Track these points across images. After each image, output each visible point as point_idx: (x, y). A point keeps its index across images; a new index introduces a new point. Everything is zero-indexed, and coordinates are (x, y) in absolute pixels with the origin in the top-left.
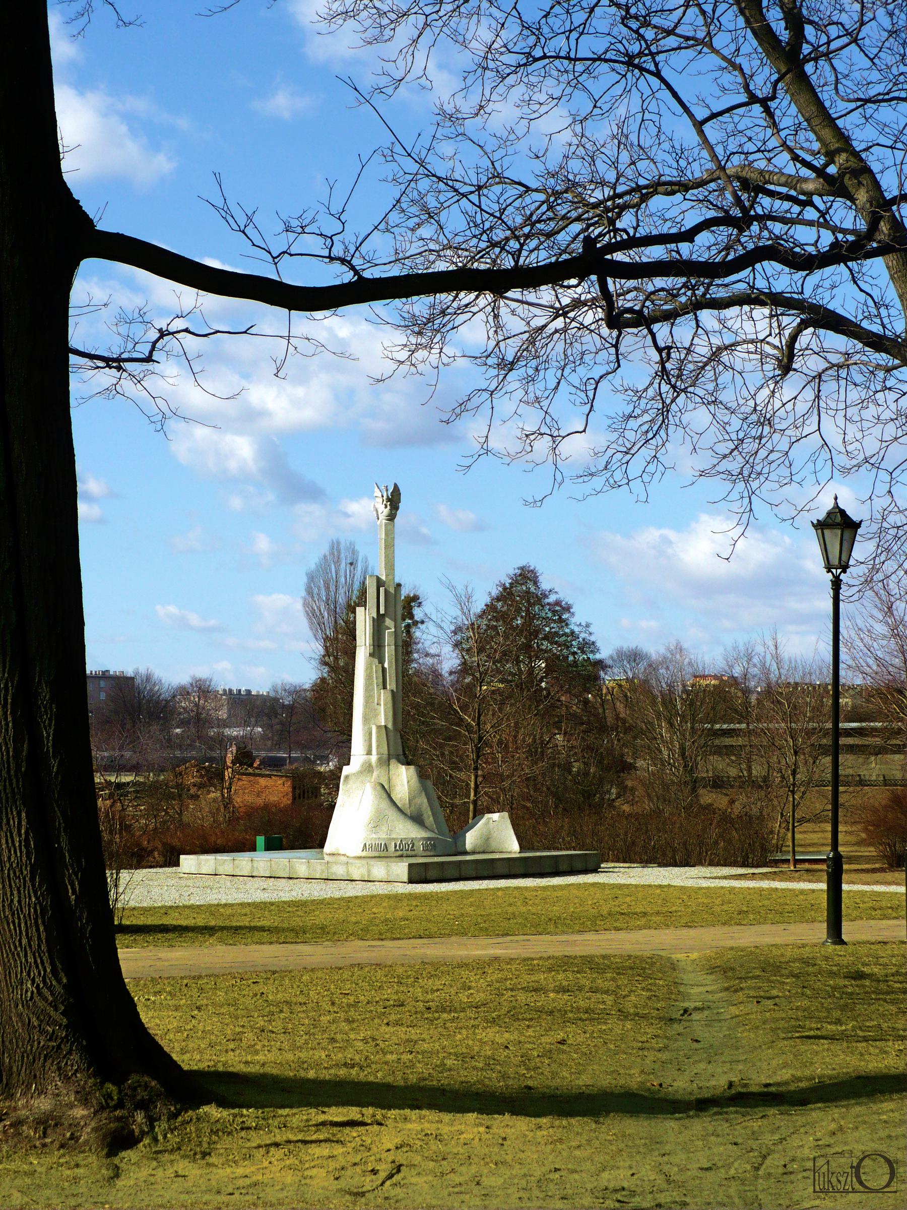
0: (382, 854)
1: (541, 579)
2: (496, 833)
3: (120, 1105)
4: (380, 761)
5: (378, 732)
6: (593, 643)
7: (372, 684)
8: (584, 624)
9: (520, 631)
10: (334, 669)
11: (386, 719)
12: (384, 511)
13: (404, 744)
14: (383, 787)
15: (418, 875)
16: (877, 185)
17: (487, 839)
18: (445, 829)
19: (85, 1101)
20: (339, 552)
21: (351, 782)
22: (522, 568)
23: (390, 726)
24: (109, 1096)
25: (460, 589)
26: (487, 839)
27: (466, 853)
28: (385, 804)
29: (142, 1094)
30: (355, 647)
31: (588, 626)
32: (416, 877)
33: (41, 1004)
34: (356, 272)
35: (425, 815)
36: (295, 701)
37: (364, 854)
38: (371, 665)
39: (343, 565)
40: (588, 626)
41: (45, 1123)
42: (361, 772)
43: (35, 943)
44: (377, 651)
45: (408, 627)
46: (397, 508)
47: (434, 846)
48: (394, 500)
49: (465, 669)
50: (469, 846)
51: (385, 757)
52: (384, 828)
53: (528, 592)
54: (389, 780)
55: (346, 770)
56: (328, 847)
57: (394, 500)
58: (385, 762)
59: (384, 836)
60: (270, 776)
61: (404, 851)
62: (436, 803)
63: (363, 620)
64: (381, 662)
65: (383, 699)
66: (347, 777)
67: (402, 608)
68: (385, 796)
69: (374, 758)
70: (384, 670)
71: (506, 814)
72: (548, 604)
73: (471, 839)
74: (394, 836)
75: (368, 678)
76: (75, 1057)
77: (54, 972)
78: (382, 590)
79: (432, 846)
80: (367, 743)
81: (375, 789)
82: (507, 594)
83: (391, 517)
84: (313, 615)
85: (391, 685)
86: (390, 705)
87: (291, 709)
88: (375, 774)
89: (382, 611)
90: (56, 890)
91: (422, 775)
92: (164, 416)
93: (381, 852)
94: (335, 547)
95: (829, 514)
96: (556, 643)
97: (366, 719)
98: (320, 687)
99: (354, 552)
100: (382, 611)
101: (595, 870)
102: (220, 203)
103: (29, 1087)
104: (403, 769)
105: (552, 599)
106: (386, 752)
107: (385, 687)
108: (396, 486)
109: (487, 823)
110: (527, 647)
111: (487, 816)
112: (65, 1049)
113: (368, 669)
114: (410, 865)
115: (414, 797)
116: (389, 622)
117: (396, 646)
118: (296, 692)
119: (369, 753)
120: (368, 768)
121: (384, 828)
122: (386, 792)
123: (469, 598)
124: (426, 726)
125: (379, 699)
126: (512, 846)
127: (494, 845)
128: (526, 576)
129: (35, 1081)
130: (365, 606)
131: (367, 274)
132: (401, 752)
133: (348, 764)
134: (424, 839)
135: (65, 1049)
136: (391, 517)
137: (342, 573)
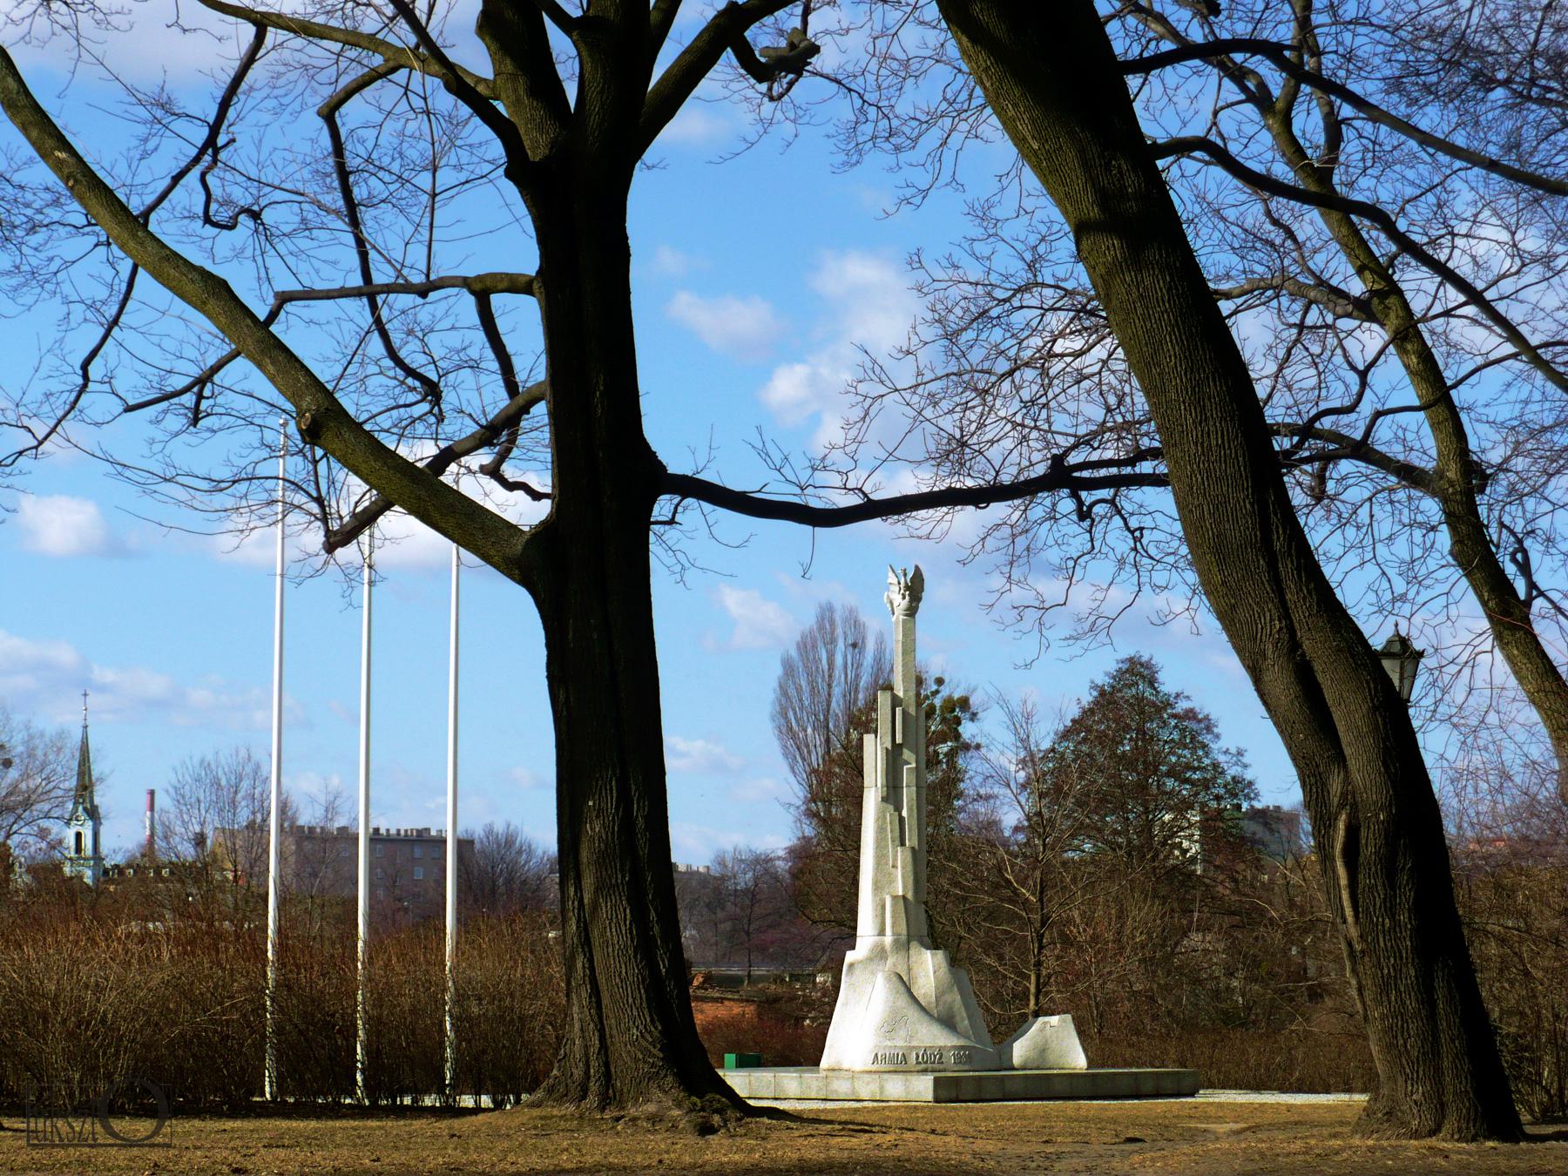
0: (900, 1068)
1: (1161, 676)
2: (1056, 1041)
3: (703, 1109)
4: (896, 942)
5: (894, 906)
6: (1250, 784)
7: (885, 839)
8: (1233, 750)
9: (1128, 762)
10: (825, 822)
11: (905, 887)
12: (901, 603)
13: (932, 919)
14: (900, 977)
15: (947, 1090)
16: (1405, 305)
17: (1043, 1050)
18: (987, 1037)
19: (679, 1105)
20: (832, 622)
21: (857, 971)
22: (1131, 660)
23: (910, 896)
24: (695, 1104)
25: (1016, 705)
26: (1043, 1050)
27: (1014, 1069)
28: (903, 1001)
29: (716, 1105)
30: (862, 788)
31: (1240, 753)
32: (943, 1094)
33: (644, 1044)
34: (865, 495)
35: (958, 1018)
36: (756, 879)
37: (875, 1067)
38: (884, 813)
39: (841, 645)
40: (1240, 753)
41: (654, 1119)
42: (870, 959)
43: (638, 1002)
44: (892, 794)
45: (952, 754)
46: (919, 599)
47: (969, 1057)
48: (915, 588)
49: (1037, 824)
50: (1016, 1061)
51: (904, 938)
52: (902, 1033)
53: (1140, 699)
54: (909, 970)
55: (850, 956)
56: (825, 1063)
57: (915, 588)
58: (903, 945)
59: (901, 1043)
60: (721, 1000)
61: (928, 1062)
62: (973, 1001)
63: (874, 752)
64: (898, 809)
65: (901, 860)
66: (851, 965)
67: (938, 725)
68: (902, 989)
69: (888, 939)
70: (901, 819)
71: (1068, 1017)
72: (1175, 716)
73: (1021, 1050)
74: (915, 1043)
75: (880, 830)
76: (670, 1078)
77: (652, 1021)
78: (898, 710)
79: (967, 1056)
80: (879, 920)
81: (889, 980)
82: (1106, 700)
83: (911, 611)
84: (789, 734)
85: (912, 840)
86: (910, 868)
87: (752, 894)
88: (890, 961)
89: (899, 740)
90: (652, 965)
91: (953, 962)
92: (683, 568)
93: (899, 1064)
94: (826, 617)
95: (1390, 642)
96: (1187, 781)
97: (877, 887)
98: (802, 854)
99: (855, 624)
100: (899, 740)
101: (1192, 1095)
102: (760, 446)
103: (637, 1100)
104: (927, 955)
105: (1182, 706)
106: (905, 932)
107: (903, 844)
108: (917, 570)
109: (1042, 1030)
110: (1142, 787)
111: (1041, 1020)
112: (662, 1073)
113: (880, 818)
114: (936, 1080)
115: (943, 993)
116: (907, 754)
117: (918, 787)
118: (762, 863)
119: (882, 932)
120: (879, 954)
121: (902, 1033)
122: (905, 985)
123: (1028, 717)
124: (965, 903)
125: (895, 860)
126: (1077, 1060)
127: (1052, 1058)
128: (1138, 671)
129: (641, 1094)
130: (876, 733)
131: (874, 497)
132: (925, 931)
133: (853, 948)
134: (955, 1047)
135: (662, 1073)
136: (911, 611)
137: (839, 660)
